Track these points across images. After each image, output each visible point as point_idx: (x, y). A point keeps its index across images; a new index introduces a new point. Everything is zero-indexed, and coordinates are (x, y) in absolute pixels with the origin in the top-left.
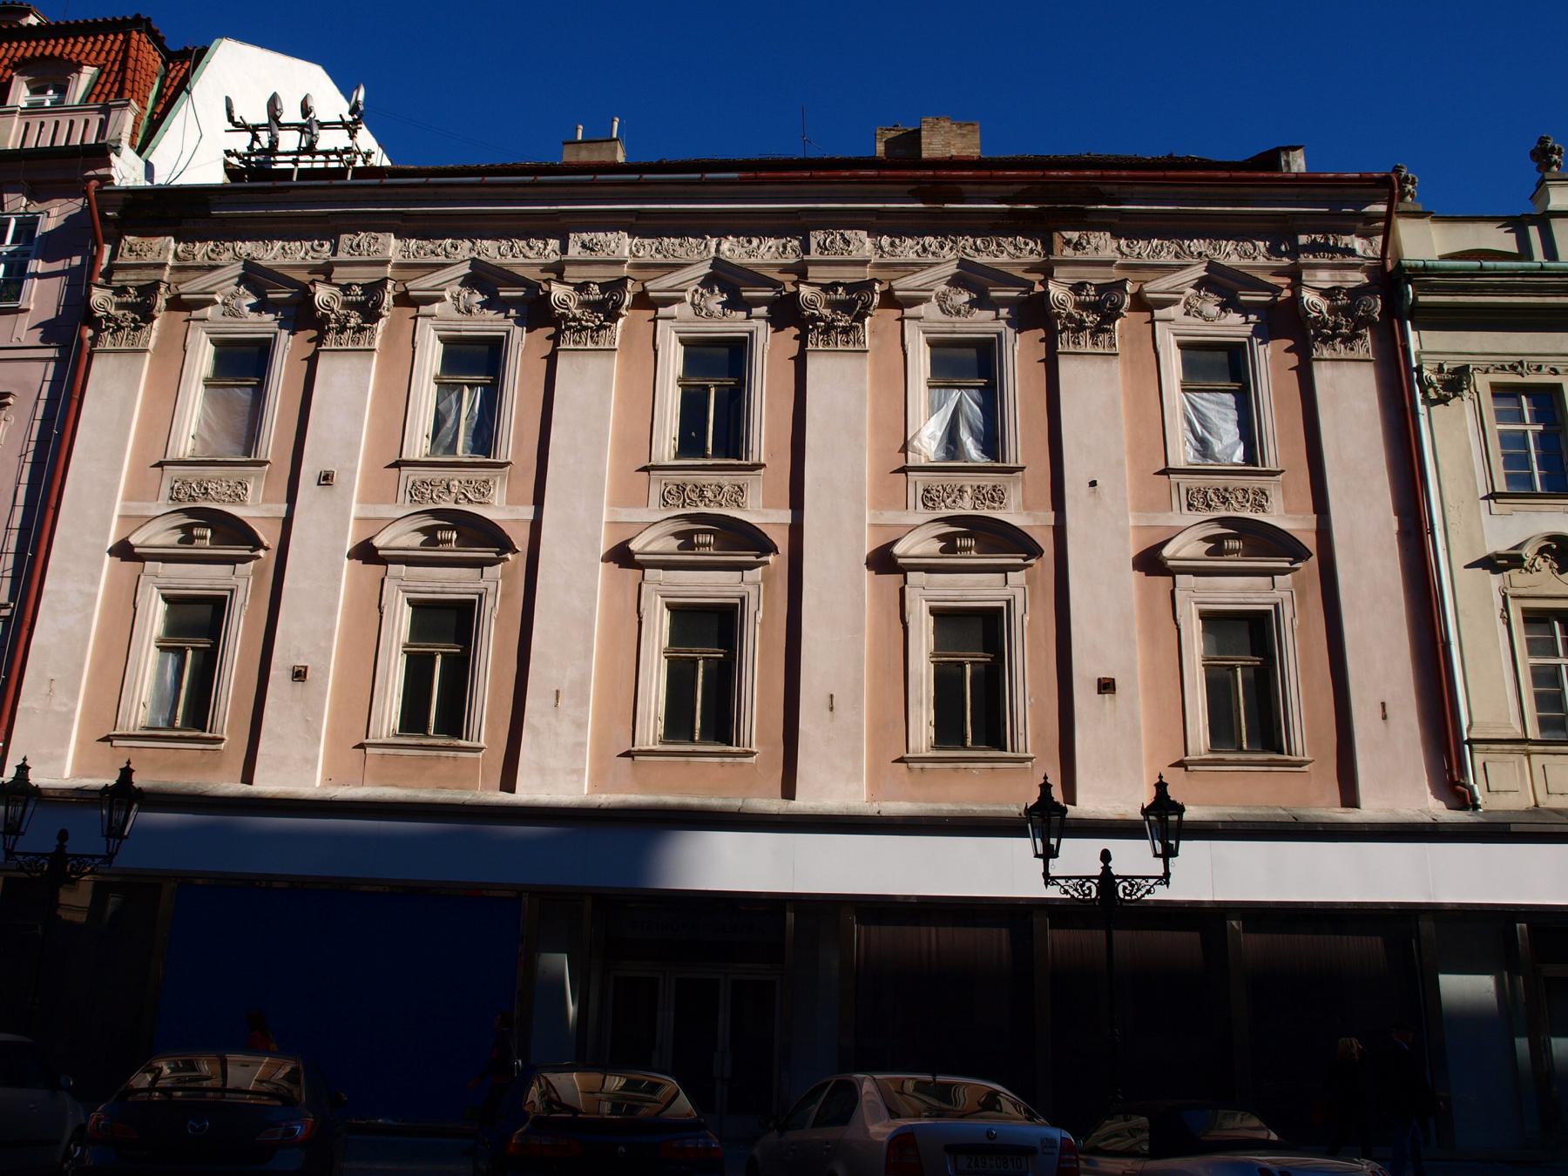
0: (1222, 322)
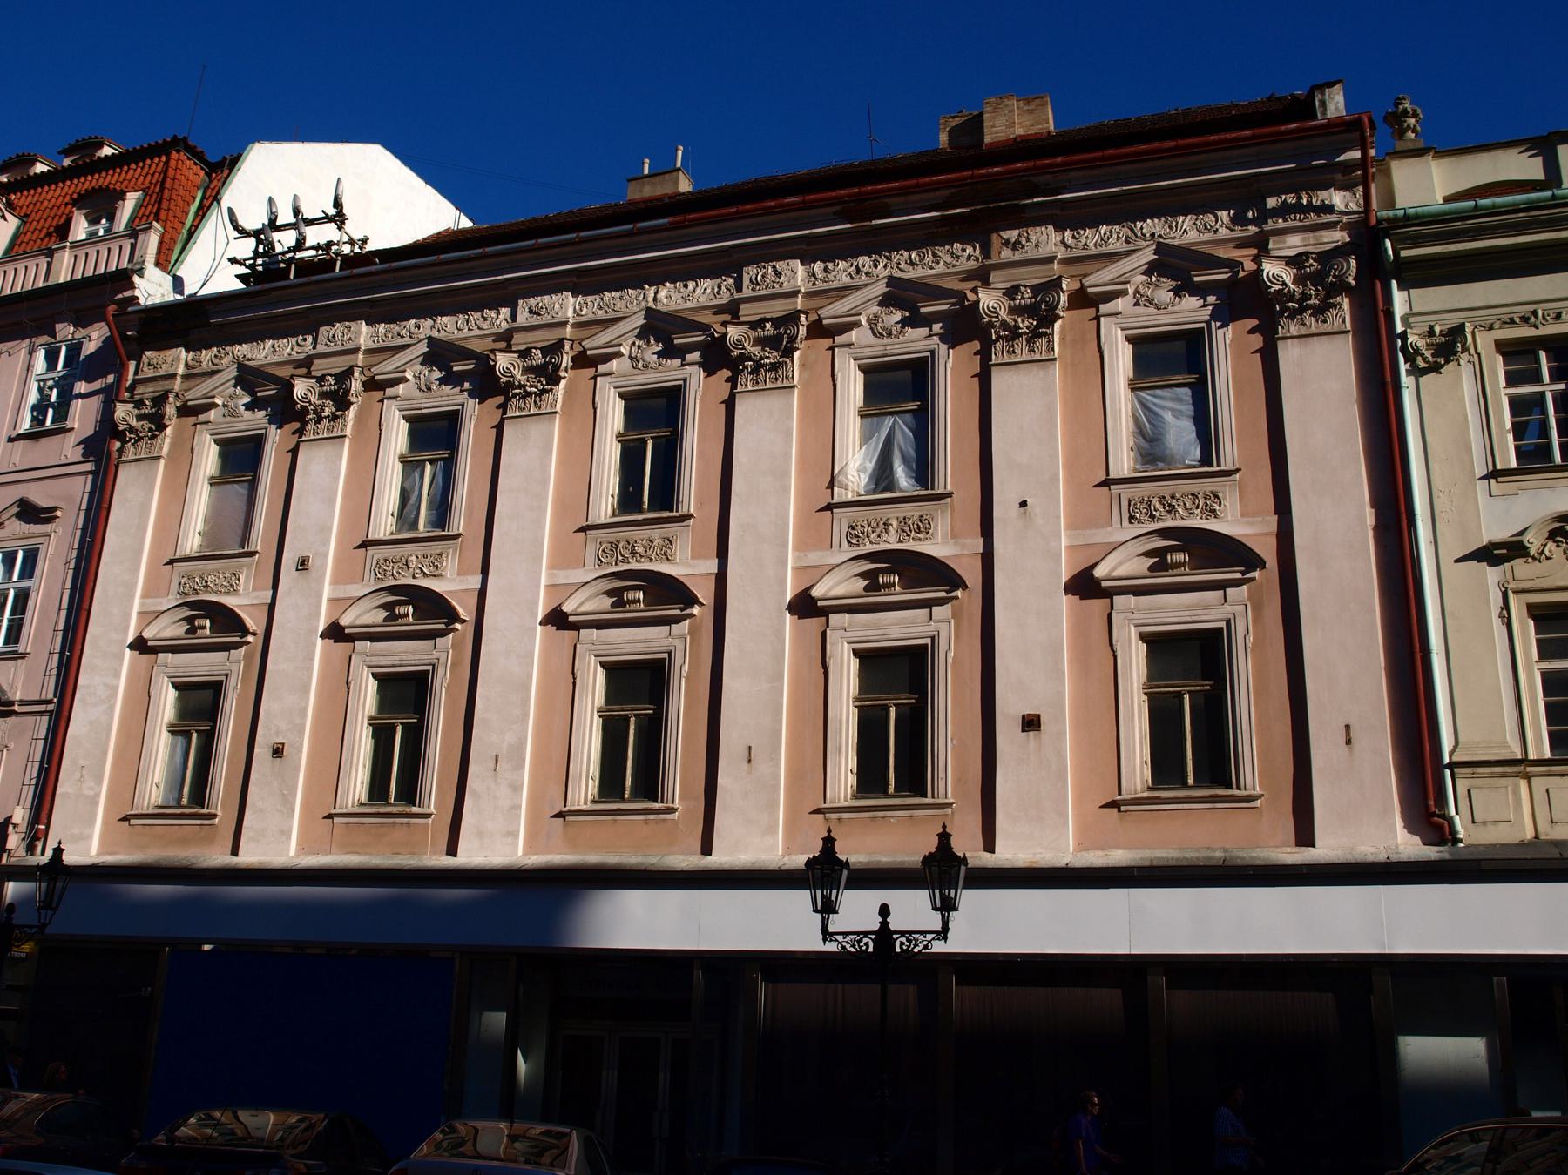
0: (1176, 308)
